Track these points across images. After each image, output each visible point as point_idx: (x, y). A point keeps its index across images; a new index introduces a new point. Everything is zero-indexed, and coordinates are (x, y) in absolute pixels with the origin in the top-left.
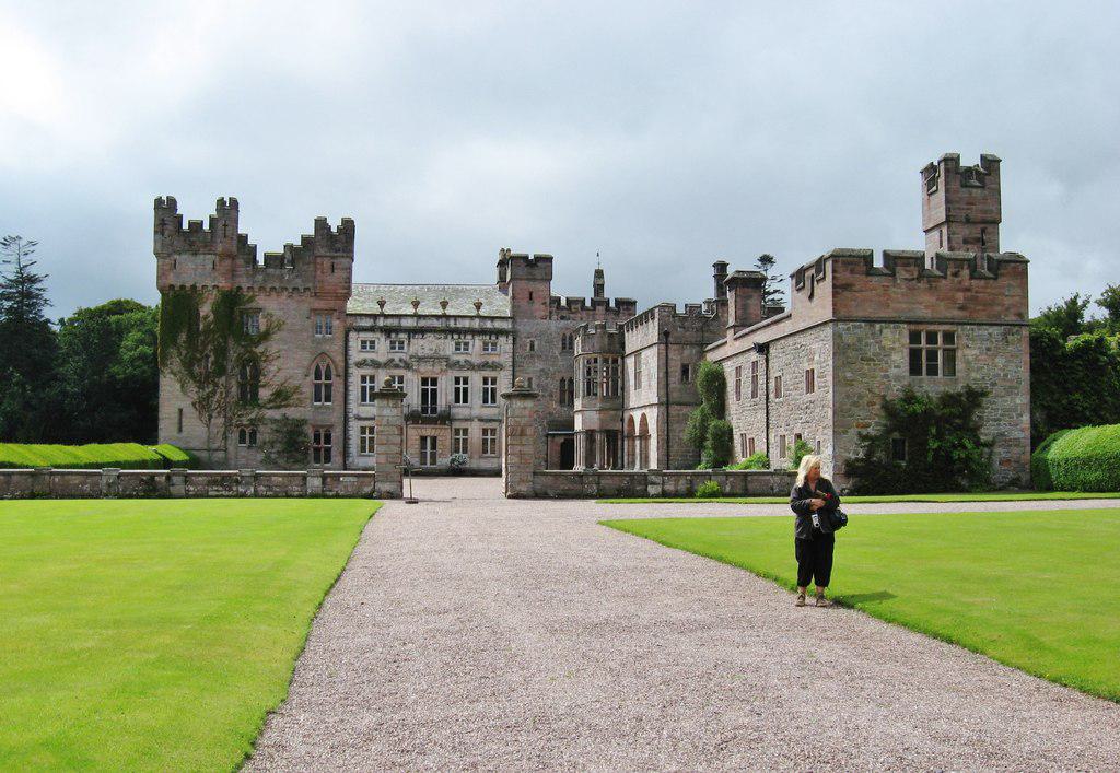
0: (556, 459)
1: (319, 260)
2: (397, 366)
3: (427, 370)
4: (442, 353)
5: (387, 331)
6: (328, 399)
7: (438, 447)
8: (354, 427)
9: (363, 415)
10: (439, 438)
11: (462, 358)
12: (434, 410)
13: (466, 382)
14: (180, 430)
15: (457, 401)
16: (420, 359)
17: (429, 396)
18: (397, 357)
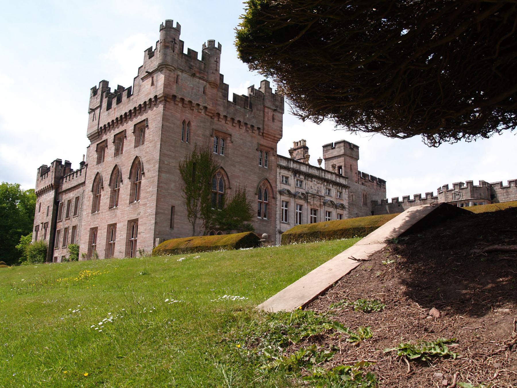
1: (266, 110)
5: (296, 172)
14: (172, 227)
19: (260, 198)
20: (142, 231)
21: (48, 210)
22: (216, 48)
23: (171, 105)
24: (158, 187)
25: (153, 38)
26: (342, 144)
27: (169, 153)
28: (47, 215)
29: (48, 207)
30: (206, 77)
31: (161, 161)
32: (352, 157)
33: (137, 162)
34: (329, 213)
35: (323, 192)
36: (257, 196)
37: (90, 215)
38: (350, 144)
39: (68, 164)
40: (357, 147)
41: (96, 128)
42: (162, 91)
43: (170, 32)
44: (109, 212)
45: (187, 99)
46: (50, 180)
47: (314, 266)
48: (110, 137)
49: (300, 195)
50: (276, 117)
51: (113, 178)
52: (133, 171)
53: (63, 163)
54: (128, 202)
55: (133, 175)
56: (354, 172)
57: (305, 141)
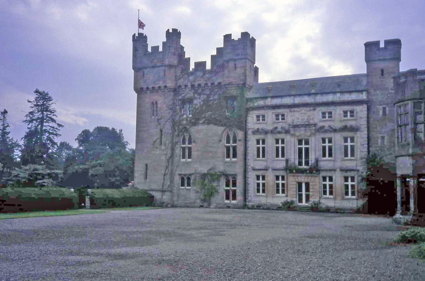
0: (266, 184)
2: (279, 133)
3: (301, 133)
4: (312, 122)
6: (235, 156)
7: (311, 190)
8: (252, 176)
9: (257, 168)
10: (311, 184)
11: (326, 125)
12: (307, 163)
13: (283, 142)
15: (324, 155)
16: (295, 126)
17: (304, 154)
18: (279, 126)
45: (150, 87)
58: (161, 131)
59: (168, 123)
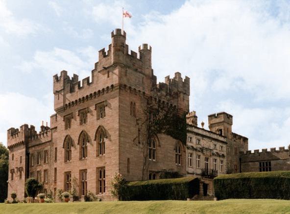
14: (128, 172)
19: (176, 152)
20: (108, 174)
21: (21, 159)
22: (148, 50)
23: (123, 92)
24: (120, 146)
25: (107, 41)
26: (222, 115)
27: (124, 124)
28: (21, 162)
29: (21, 157)
30: (143, 71)
31: (120, 130)
32: (228, 123)
33: (100, 130)
34: (216, 160)
35: (212, 147)
36: (175, 151)
37: (63, 163)
38: (227, 114)
39: (33, 127)
40: (232, 117)
41: (62, 105)
42: (117, 82)
43: (119, 37)
44: (79, 162)
45: (133, 87)
46: (21, 138)
47: (5, 173)
48: (75, 111)
49: (199, 149)
50: (185, 99)
51: (80, 139)
52: (97, 135)
53: (29, 127)
54: (95, 155)
55: (97, 138)
56: (229, 133)
57: (195, 112)
58: (139, 130)
59: (143, 125)
